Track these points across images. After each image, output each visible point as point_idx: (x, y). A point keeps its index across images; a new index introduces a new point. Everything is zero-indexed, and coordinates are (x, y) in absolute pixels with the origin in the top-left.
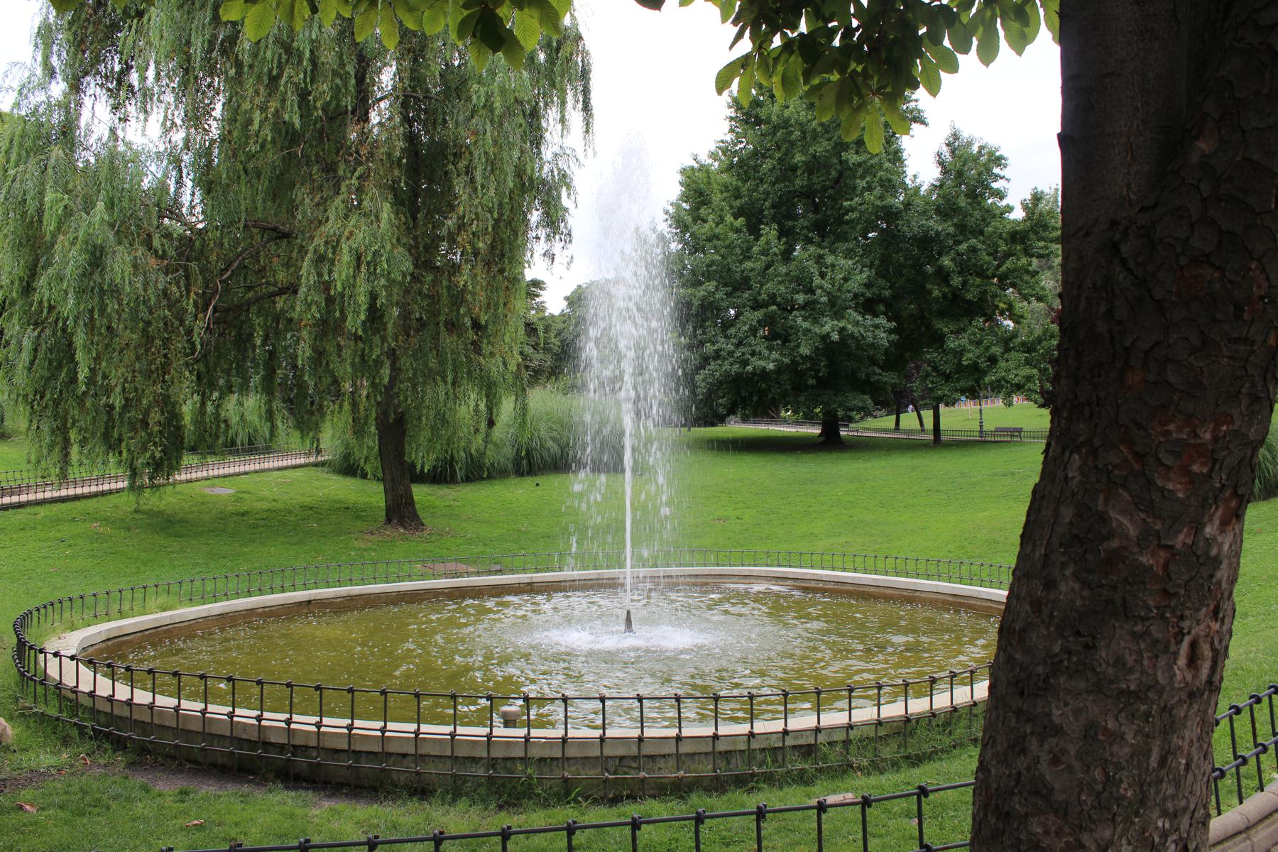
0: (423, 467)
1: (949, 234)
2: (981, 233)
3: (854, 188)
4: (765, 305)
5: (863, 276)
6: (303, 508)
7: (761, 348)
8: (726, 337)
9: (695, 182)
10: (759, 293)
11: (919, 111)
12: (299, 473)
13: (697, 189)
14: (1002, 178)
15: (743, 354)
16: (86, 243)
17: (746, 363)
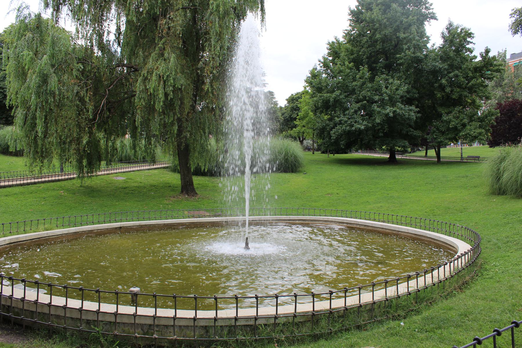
0: (204, 169)
1: (445, 69)
2: (461, 68)
3: (403, 49)
4: (361, 101)
5: (405, 88)
6: (152, 186)
7: (359, 120)
8: (344, 115)
9: (334, 48)
10: (359, 96)
11: (434, 14)
12: (156, 171)
13: (335, 50)
14: (471, 43)
15: (351, 122)
16: (40, 73)
17: (352, 126)
